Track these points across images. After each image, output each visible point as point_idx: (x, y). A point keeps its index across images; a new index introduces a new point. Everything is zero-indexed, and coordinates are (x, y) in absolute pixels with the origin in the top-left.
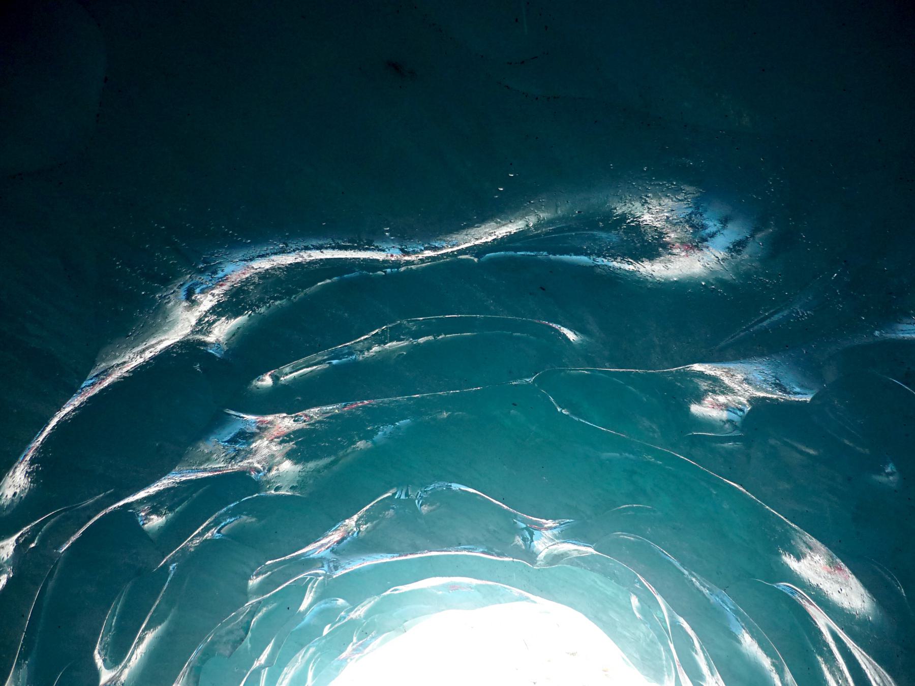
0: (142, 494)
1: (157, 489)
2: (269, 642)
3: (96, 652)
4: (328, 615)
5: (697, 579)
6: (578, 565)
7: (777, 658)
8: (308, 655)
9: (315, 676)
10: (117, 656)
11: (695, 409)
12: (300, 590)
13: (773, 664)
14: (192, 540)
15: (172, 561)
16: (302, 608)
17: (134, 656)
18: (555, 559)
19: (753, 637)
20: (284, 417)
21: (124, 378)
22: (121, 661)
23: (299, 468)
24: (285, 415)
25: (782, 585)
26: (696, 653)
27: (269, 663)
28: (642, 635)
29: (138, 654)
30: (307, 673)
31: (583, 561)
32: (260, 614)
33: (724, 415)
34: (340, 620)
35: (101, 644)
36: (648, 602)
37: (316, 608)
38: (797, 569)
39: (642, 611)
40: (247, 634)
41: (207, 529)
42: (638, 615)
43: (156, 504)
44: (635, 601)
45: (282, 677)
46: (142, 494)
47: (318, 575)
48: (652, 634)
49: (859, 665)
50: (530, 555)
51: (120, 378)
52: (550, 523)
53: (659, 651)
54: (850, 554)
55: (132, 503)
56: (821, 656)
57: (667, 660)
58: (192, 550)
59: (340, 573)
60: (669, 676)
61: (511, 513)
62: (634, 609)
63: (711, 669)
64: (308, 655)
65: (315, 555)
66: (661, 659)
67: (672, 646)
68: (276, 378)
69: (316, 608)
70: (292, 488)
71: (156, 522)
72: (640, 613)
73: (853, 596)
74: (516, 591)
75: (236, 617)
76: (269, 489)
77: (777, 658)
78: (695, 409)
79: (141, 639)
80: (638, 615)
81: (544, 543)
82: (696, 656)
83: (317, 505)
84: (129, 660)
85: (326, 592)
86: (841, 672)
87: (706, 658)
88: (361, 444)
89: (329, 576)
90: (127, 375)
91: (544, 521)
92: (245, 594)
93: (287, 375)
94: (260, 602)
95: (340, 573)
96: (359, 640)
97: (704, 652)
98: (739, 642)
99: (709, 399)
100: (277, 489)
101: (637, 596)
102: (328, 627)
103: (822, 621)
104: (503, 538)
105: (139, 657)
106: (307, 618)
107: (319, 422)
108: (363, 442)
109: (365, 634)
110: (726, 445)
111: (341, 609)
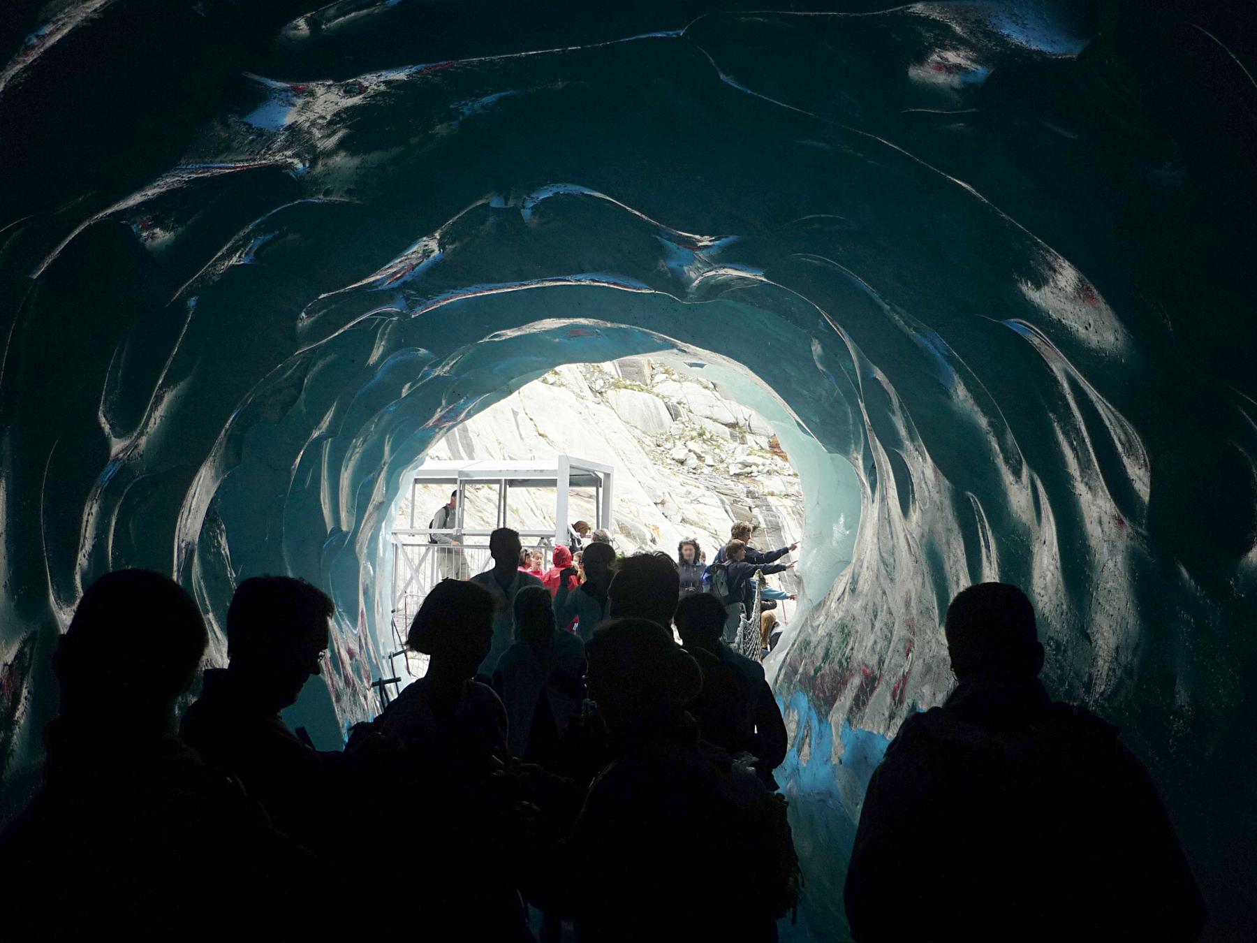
0: (136, 199)
1: (157, 190)
2: (331, 405)
3: (100, 414)
4: (408, 371)
5: (901, 316)
6: (743, 300)
7: (997, 416)
8: (383, 423)
9: (393, 450)
10: (128, 421)
11: (916, 73)
12: (366, 336)
13: (991, 424)
14: (214, 265)
15: (190, 293)
16: (373, 359)
17: (152, 420)
18: (713, 289)
19: (968, 389)
20: (330, 86)
21: (92, 20)
22: (137, 426)
23: (356, 161)
24: (331, 82)
25: (1017, 324)
26: (893, 412)
27: (331, 431)
28: (824, 393)
29: (157, 418)
30: (383, 446)
31: (746, 292)
32: (316, 369)
33: (955, 80)
34: (423, 378)
35: (105, 403)
36: (834, 349)
37: (389, 361)
38: (1038, 300)
39: (825, 360)
40: (300, 392)
41: (229, 254)
42: (820, 367)
43: (156, 211)
44: (817, 348)
45: (350, 451)
46: (136, 199)
47: (390, 315)
48: (838, 391)
49: (1102, 421)
50: (677, 284)
51: (85, 20)
52: (705, 241)
53: (846, 413)
54: (1100, 279)
55: (125, 210)
56: (1053, 411)
57: (855, 424)
58: (216, 279)
59: (419, 312)
60: (856, 444)
61: (653, 225)
62: (815, 358)
63: (910, 433)
64: (383, 423)
65: (386, 286)
66: (846, 422)
67: (862, 405)
68: (312, 23)
69: (389, 361)
70: (349, 192)
71: (162, 236)
72: (822, 363)
73: (1099, 328)
74: (658, 336)
75: (284, 370)
76: (317, 192)
77: (997, 416)
78: (915, 73)
79: (159, 399)
80: (820, 367)
81: (698, 269)
82: (893, 418)
83: (381, 217)
84: (146, 424)
85: (405, 336)
86: (1078, 431)
87: (906, 419)
88: (441, 129)
89: (407, 316)
90: (95, 16)
91: (698, 237)
92: (294, 340)
93: (329, 20)
94: (313, 351)
95: (419, 312)
96: (449, 403)
97: (903, 412)
98: (949, 397)
99: (935, 57)
100: (327, 193)
101: (821, 341)
102: (408, 386)
103: (1059, 365)
104: (643, 257)
105: (158, 421)
106: (379, 374)
107: (382, 94)
108: (445, 125)
109: (455, 396)
110: (954, 126)
111: (423, 362)
